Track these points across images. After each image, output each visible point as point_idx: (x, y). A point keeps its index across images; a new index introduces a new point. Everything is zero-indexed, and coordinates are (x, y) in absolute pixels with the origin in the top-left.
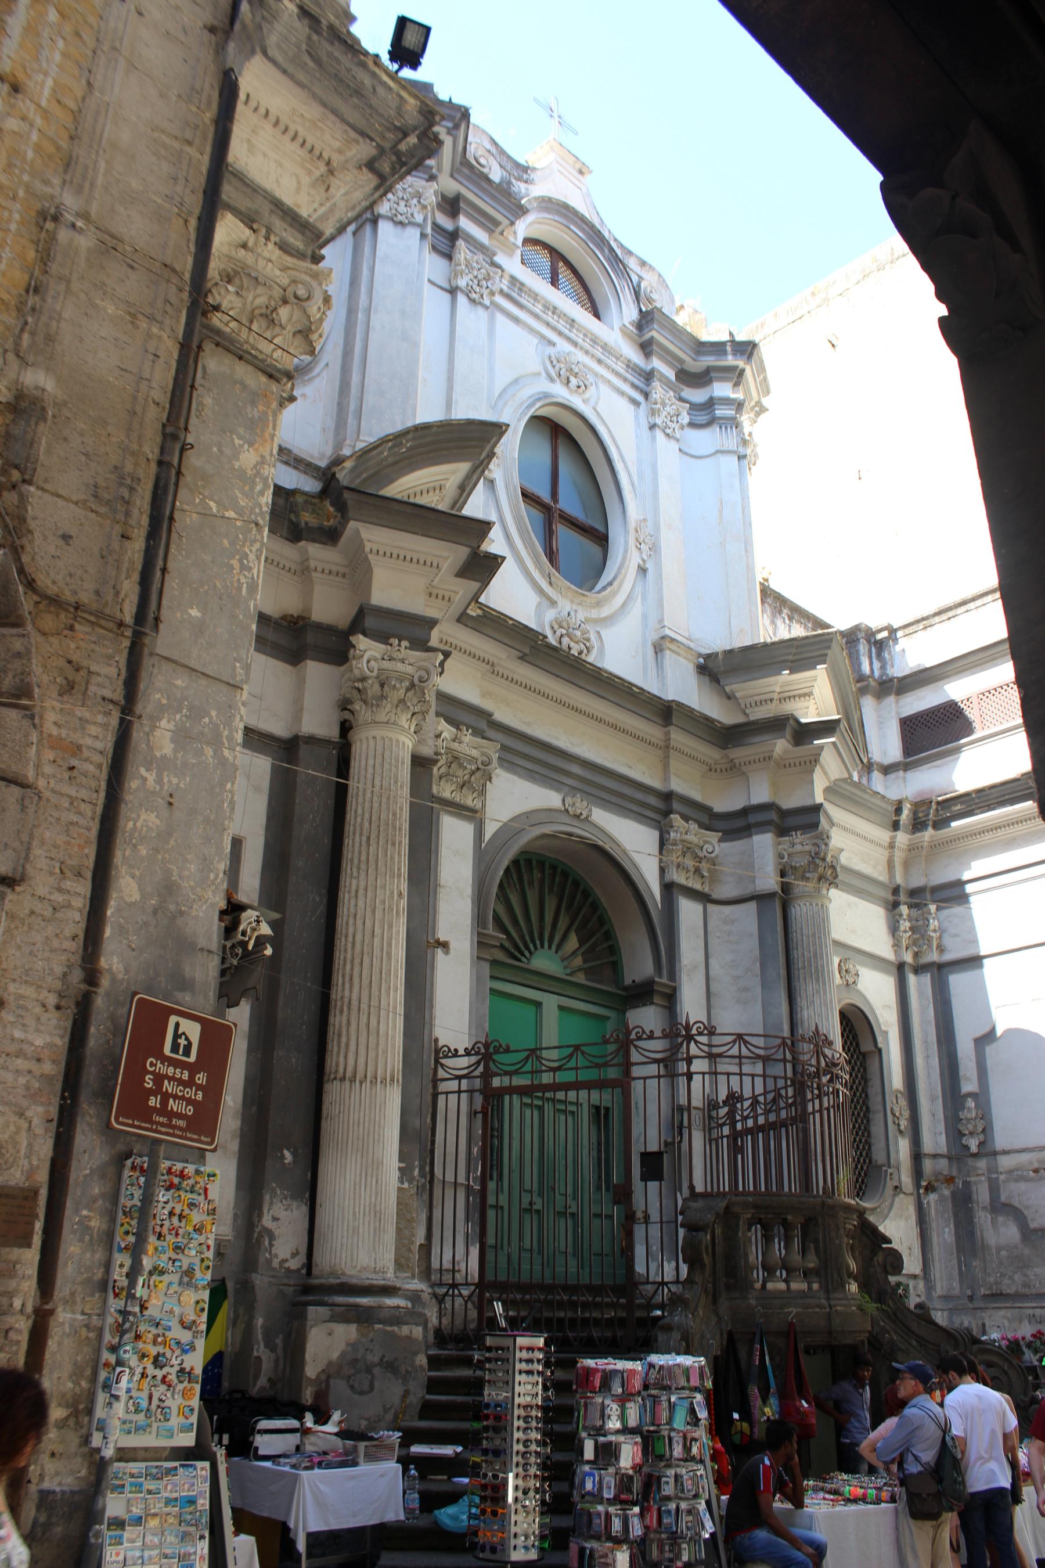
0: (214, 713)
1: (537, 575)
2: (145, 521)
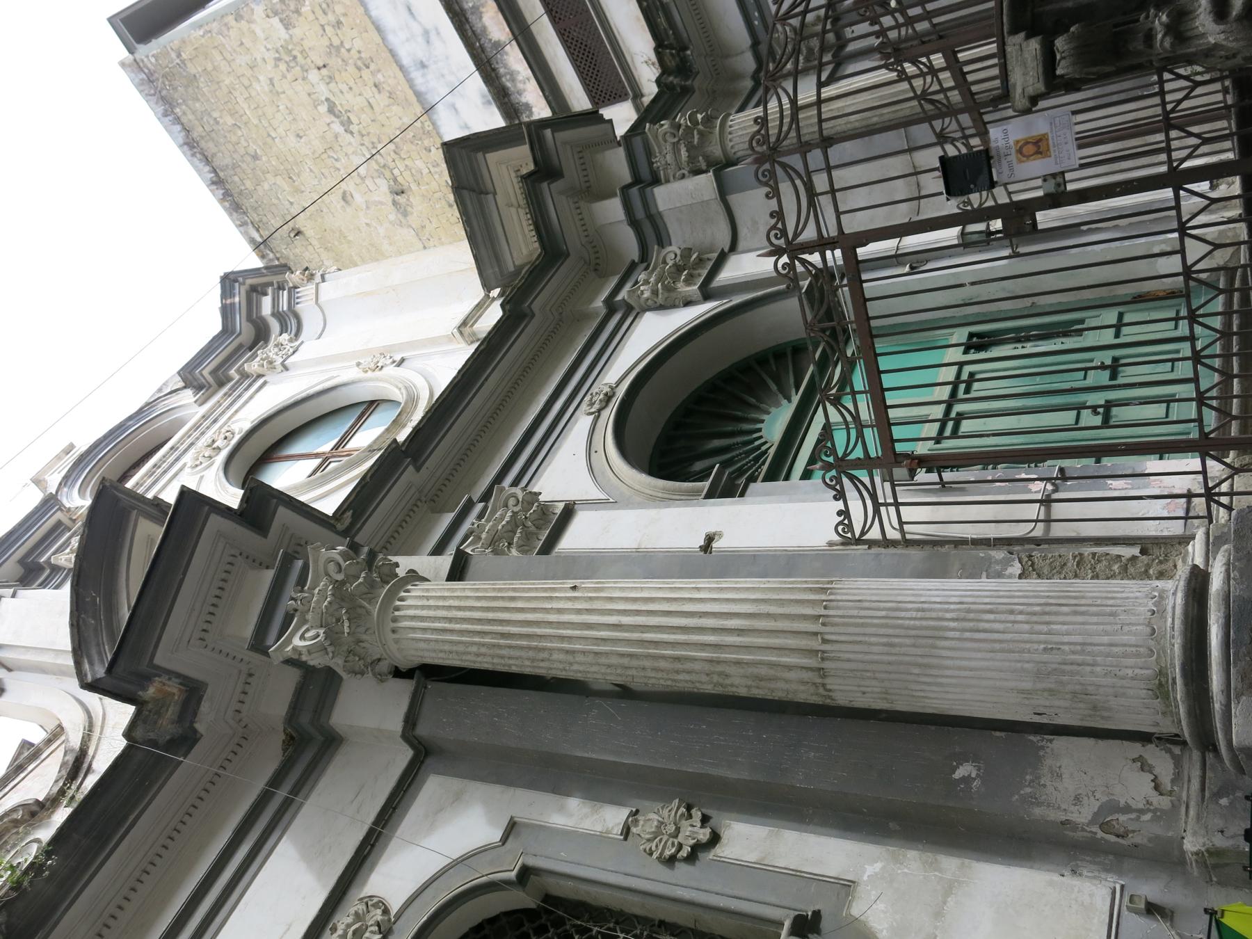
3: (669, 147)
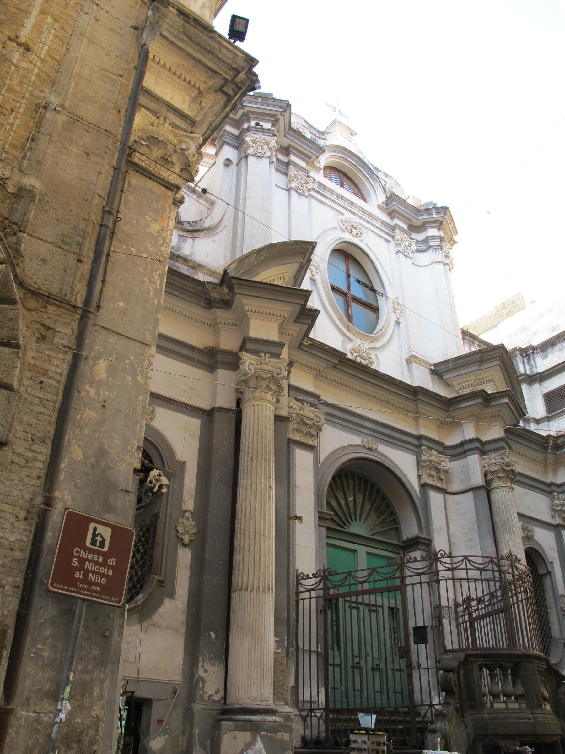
0: (132, 358)
1: (341, 326)
2: (92, 254)
3: (498, 461)
